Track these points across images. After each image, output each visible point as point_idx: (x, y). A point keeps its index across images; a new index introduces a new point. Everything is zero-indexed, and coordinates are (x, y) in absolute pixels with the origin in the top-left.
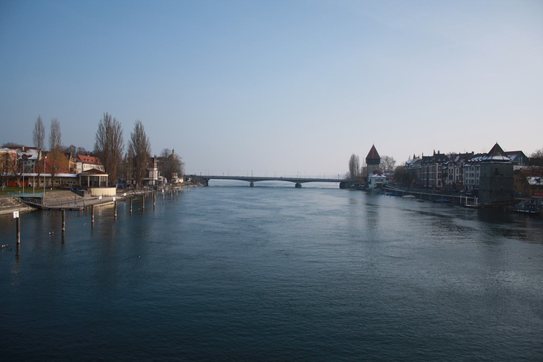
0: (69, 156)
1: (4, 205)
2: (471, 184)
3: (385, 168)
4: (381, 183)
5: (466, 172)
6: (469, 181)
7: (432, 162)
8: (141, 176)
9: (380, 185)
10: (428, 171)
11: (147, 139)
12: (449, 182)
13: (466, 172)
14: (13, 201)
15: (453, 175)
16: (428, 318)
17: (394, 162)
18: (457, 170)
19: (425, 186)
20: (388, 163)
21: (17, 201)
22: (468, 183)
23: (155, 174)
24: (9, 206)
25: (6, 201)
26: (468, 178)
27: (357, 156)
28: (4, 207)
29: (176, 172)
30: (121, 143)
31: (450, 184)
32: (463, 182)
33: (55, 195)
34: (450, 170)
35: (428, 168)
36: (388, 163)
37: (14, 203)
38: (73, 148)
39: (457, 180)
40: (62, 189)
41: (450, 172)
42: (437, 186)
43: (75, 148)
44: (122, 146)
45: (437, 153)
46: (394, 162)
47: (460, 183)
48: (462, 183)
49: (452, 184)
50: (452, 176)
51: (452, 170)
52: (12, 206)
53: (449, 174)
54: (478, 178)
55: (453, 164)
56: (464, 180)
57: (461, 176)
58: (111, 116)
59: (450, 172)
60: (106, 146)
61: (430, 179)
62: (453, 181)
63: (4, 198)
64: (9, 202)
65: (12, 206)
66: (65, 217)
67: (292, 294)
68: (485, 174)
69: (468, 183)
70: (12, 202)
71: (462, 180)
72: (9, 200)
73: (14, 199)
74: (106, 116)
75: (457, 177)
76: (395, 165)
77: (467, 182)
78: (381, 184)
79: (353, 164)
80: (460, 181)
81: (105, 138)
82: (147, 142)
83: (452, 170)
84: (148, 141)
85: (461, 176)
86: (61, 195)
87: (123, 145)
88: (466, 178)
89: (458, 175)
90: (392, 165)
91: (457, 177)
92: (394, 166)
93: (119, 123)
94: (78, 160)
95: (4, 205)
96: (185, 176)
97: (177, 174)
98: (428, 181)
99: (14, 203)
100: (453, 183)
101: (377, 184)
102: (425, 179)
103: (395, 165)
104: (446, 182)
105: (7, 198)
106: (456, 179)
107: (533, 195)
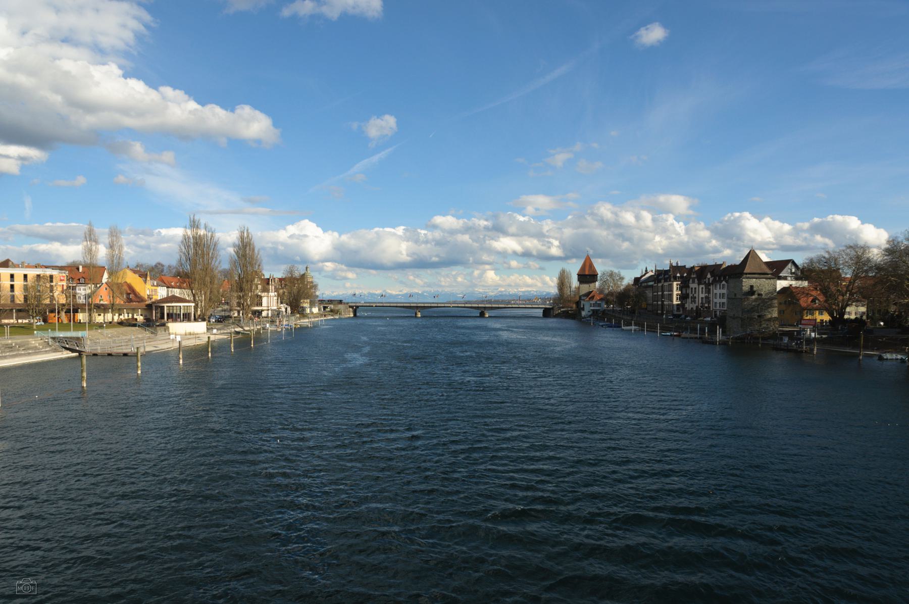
0: (146, 278)
1: (23, 350)
2: (721, 309)
3: (609, 286)
4: (598, 308)
5: (715, 291)
6: (718, 305)
7: (668, 278)
8: (251, 305)
9: (597, 312)
10: (663, 291)
11: (256, 251)
12: (691, 306)
13: (715, 291)
14: (39, 344)
15: (696, 295)
16: (361, 551)
17: (622, 279)
18: (702, 288)
19: (659, 312)
20: (613, 280)
21: (46, 343)
22: (718, 308)
23: (270, 302)
24: (30, 351)
25: (28, 343)
26: (718, 300)
27: (568, 270)
28: (23, 352)
29: (307, 298)
30: (216, 258)
31: (692, 308)
32: (711, 305)
33: (111, 333)
34: (692, 288)
35: (662, 286)
36: (613, 280)
37: (41, 347)
38: (160, 266)
39: (702, 303)
40: (480, 327)
41: (692, 292)
42: (676, 313)
43: (163, 266)
44: (217, 262)
45: (674, 264)
46: (622, 279)
47: (706, 307)
48: (709, 307)
49: (695, 309)
50: (695, 298)
51: (695, 288)
52: (37, 351)
53: (691, 295)
54: (725, 300)
55: (696, 280)
56: (711, 302)
57: (707, 298)
58: (199, 221)
59: (692, 292)
60: (193, 263)
61: (665, 303)
62: (697, 304)
63: (26, 340)
64: (32, 345)
65: (37, 351)
66: (85, 367)
67: (387, 482)
68: (735, 295)
69: (718, 308)
70: (37, 345)
71: (709, 302)
72: (33, 342)
73: (42, 341)
74: (192, 219)
75: (702, 298)
76: (623, 283)
77: (716, 306)
78: (599, 310)
79: (562, 283)
80: (706, 305)
81: (192, 252)
82: (257, 257)
83: (695, 288)
84: (258, 254)
85: (707, 298)
86: (122, 334)
87: (218, 260)
88: (715, 300)
89: (703, 296)
90: (619, 283)
91: (702, 298)
92: (622, 285)
93: (213, 229)
94: (160, 283)
95: (23, 350)
96: (322, 301)
97: (308, 301)
98: (663, 305)
99: (41, 347)
100: (697, 307)
101: (593, 310)
102: (660, 303)
103: (623, 283)
104: (686, 306)
105: (31, 340)
106: (700, 302)
107: (801, 324)
